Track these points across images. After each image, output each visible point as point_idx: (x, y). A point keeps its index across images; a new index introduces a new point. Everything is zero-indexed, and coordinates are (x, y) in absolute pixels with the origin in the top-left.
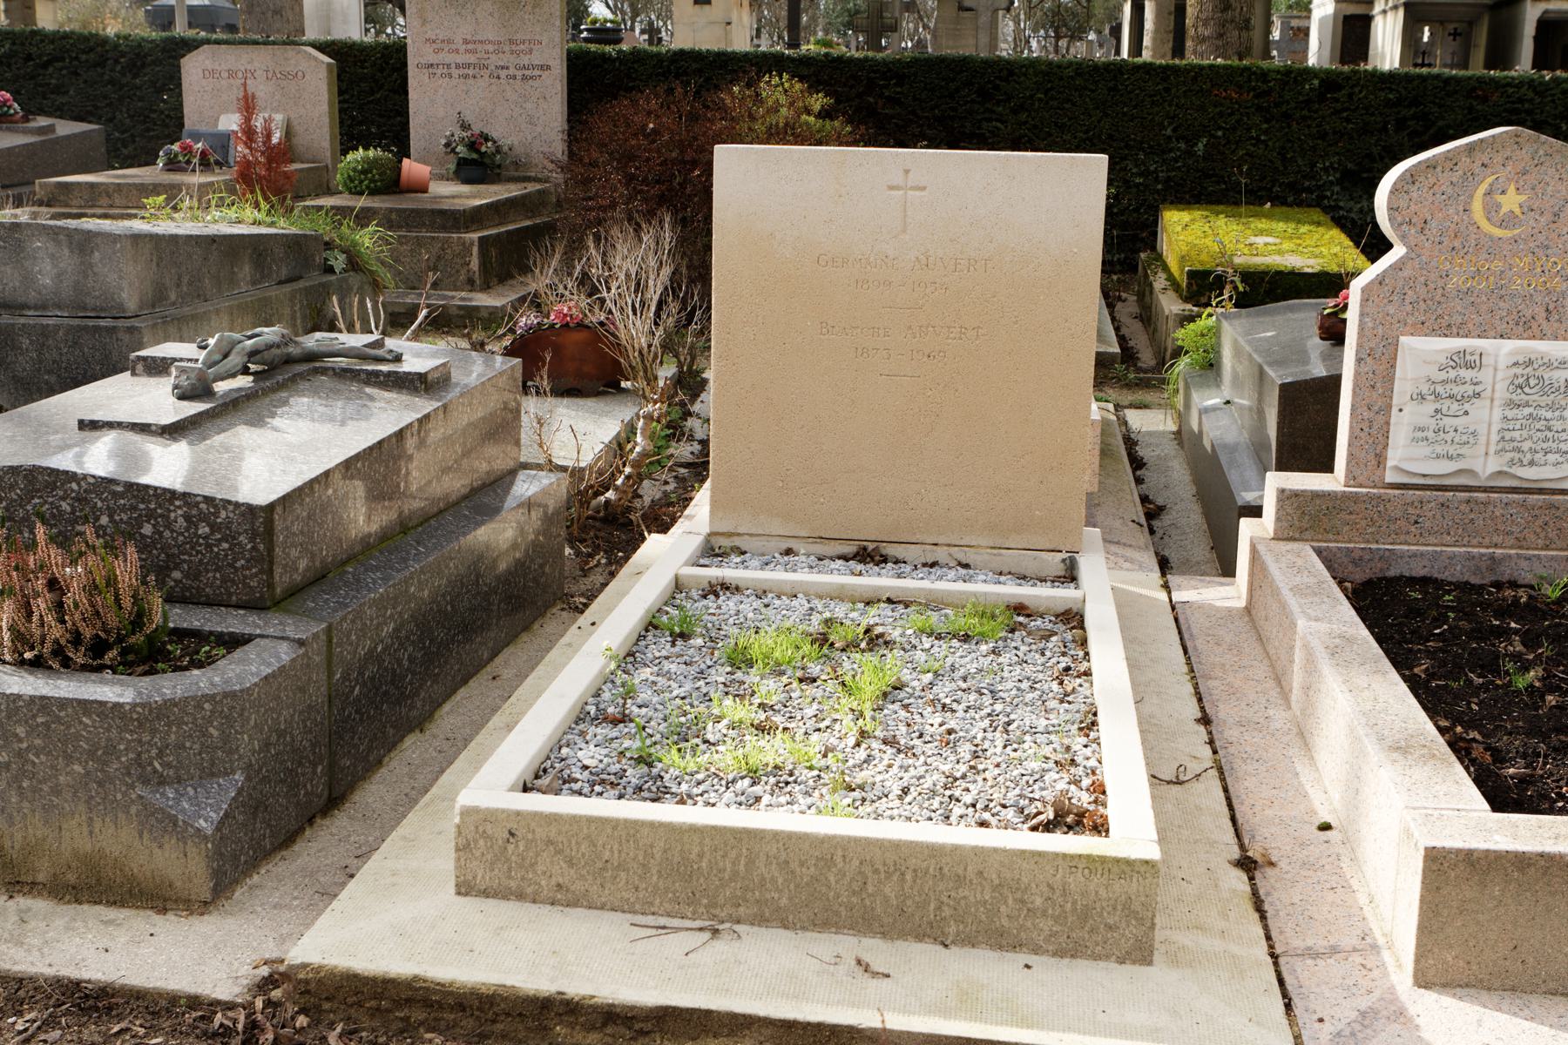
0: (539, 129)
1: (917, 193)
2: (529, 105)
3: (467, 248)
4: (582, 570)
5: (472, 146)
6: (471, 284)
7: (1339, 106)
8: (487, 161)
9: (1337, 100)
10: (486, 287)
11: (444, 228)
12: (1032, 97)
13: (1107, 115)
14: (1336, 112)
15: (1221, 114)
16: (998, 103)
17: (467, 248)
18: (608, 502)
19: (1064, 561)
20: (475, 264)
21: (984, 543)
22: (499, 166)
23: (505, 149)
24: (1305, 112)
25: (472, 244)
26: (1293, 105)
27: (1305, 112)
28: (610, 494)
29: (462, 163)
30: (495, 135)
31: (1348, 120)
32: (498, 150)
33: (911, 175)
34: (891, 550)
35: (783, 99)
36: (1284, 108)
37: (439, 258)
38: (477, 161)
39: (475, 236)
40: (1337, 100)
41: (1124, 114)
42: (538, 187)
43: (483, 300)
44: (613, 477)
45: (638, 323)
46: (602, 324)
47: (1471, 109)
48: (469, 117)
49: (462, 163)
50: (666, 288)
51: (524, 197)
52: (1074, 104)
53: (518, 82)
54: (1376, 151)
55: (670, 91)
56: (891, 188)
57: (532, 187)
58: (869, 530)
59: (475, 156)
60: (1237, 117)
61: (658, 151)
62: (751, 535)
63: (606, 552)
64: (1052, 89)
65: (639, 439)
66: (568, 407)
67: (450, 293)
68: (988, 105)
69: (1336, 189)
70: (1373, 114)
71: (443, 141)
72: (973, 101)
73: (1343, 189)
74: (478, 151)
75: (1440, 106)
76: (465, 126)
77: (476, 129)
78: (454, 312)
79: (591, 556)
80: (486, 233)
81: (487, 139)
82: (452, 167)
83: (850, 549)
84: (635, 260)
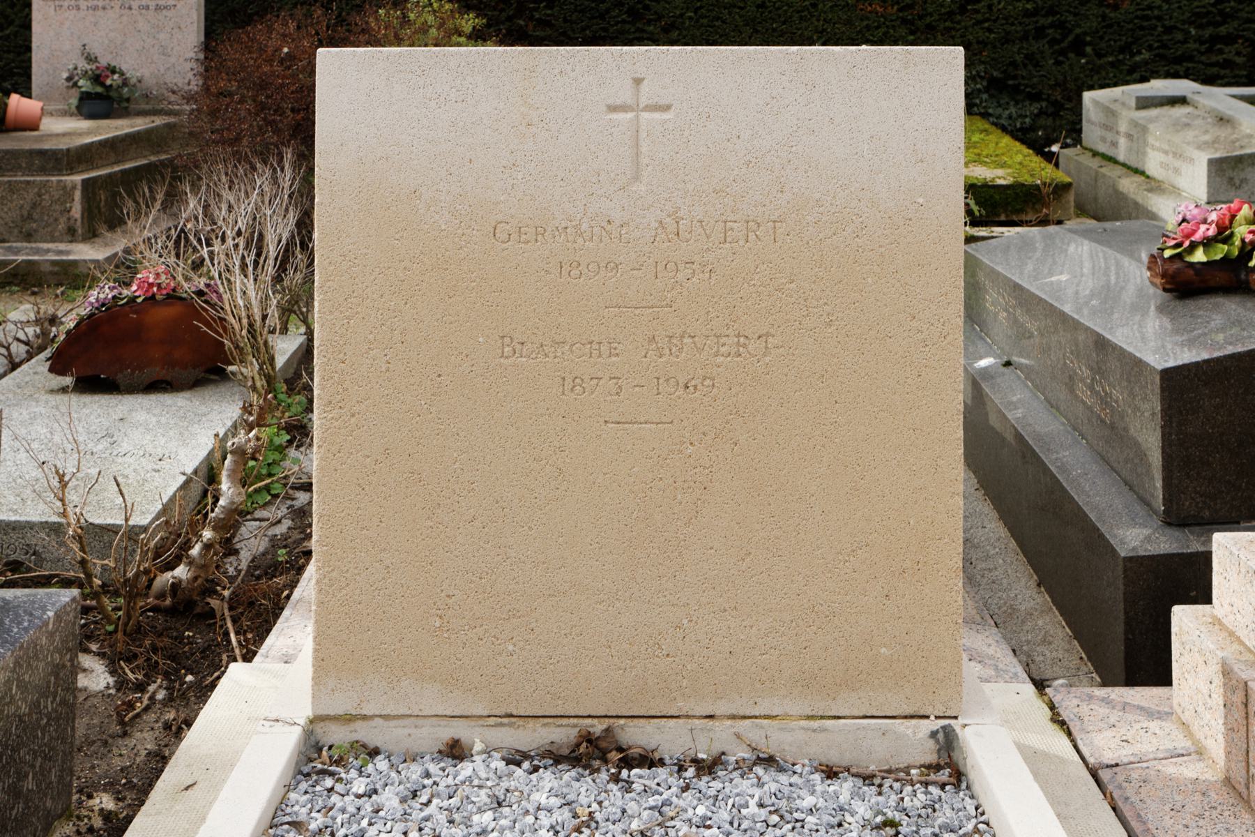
0: (173, 60)
1: (657, 115)
2: (162, 36)
3: (67, 192)
4: (122, 723)
5: (97, 79)
6: (71, 234)
7: (979, 17)
8: (113, 94)
9: (977, 11)
10: (91, 235)
11: (43, 170)
12: (682, 15)
13: (757, 31)
14: (979, 23)
15: (868, 27)
16: (649, 22)
17: (67, 192)
18: (176, 586)
19: (934, 734)
20: (77, 210)
21: (795, 708)
22: (128, 100)
23: (133, 81)
24: (948, 24)
25: (74, 188)
26: (936, 17)
27: (948, 24)
28: (181, 572)
29: (85, 97)
30: (124, 68)
31: (990, 30)
32: (125, 83)
33: (645, 87)
34: (637, 735)
35: (431, 19)
36: (928, 20)
37: (34, 206)
38: (102, 94)
39: (78, 178)
40: (977, 11)
41: (774, 30)
42: (172, 120)
43: (85, 252)
44: (187, 546)
45: (250, 284)
46: (200, 293)
47: (1104, 17)
48: (96, 49)
49: (85, 97)
50: (293, 237)
51: (149, 132)
52: (724, 22)
53: (151, 12)
54: (1019, 58)
55: (309, 15)
56: (613, 109)
57: (159, 121)
58: (591, 695)
59: (99, 89)
60: (883, 30)
61: (294, 76)
62: (386, 717)
63: (166, 675)
64: (701, 7)
65: (225, 485)
66: (148, 411)
67: (45, 246)
68: (639, 25)
69: (985, 96)
70: (1013, 24)
71: (65, 75)
72: (624, 22)
73: (991, 96)
74: (103, 85)
75: (1075, 15)
76: (90, 59)
77: (103, 62)
78: (47, 268)
79: (141, 687)
80: (86, 176)
81: (113, 72)
82: (74, 102)
83: (562, 735)
84: (245, 204)
